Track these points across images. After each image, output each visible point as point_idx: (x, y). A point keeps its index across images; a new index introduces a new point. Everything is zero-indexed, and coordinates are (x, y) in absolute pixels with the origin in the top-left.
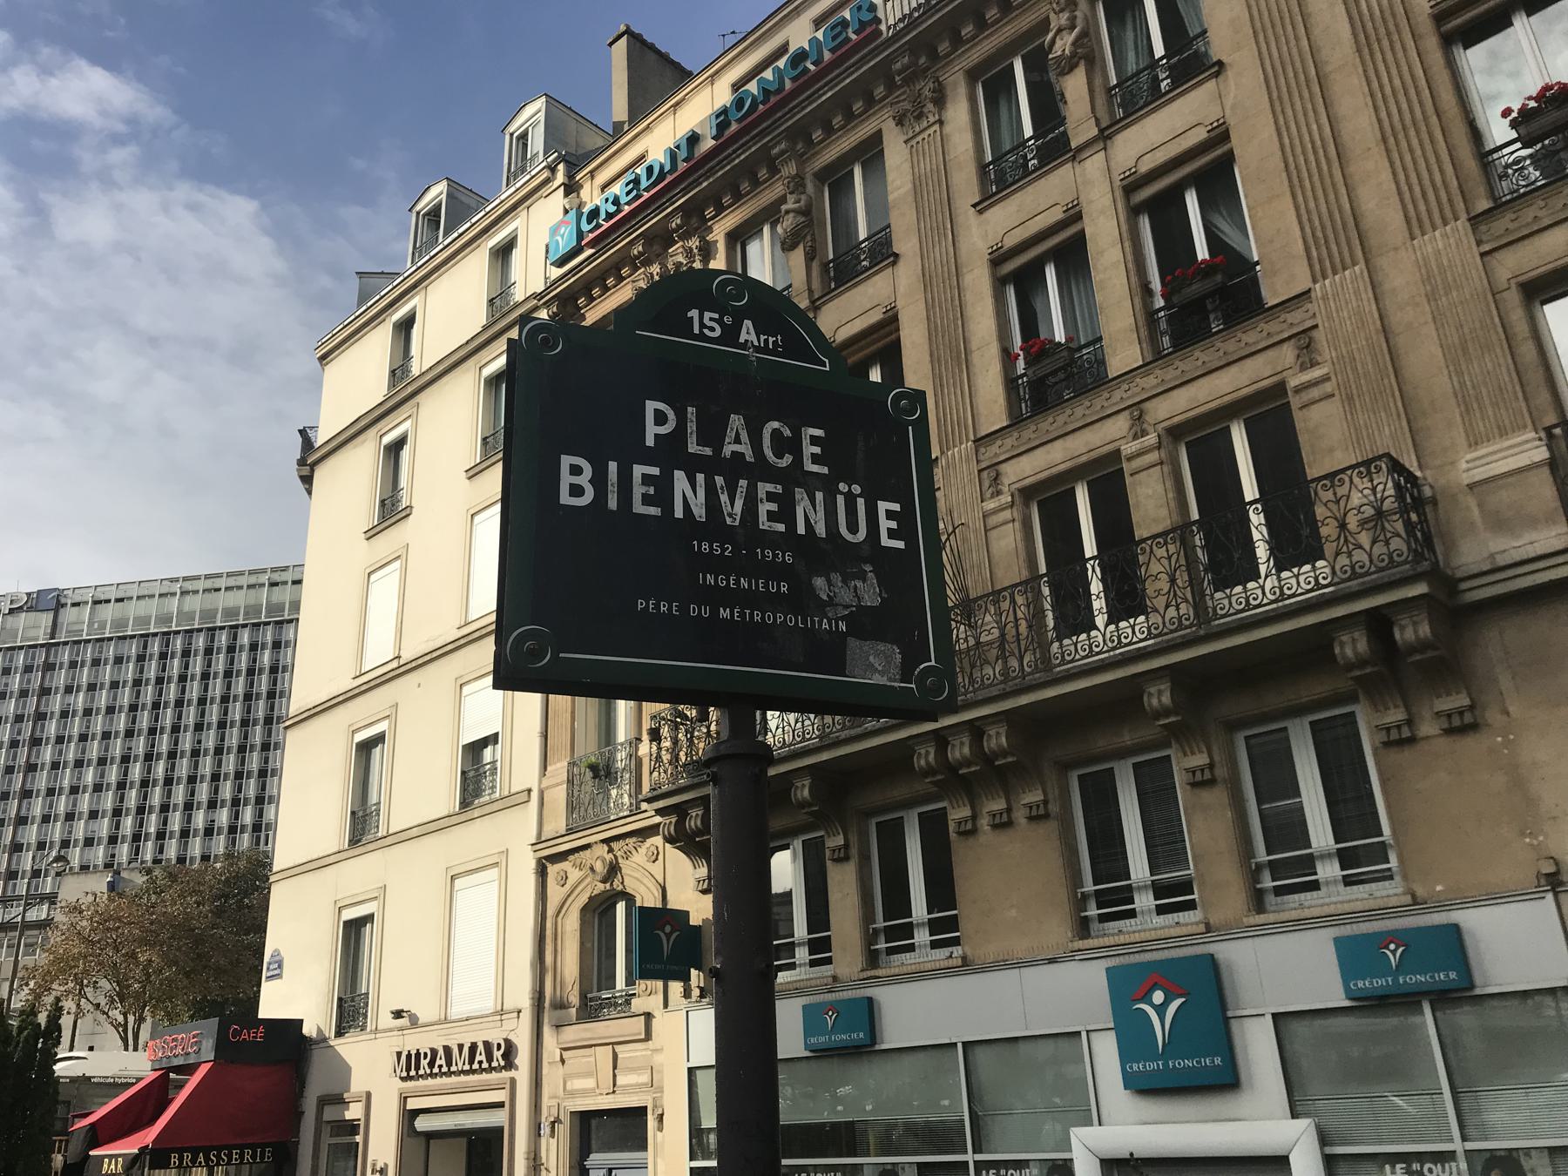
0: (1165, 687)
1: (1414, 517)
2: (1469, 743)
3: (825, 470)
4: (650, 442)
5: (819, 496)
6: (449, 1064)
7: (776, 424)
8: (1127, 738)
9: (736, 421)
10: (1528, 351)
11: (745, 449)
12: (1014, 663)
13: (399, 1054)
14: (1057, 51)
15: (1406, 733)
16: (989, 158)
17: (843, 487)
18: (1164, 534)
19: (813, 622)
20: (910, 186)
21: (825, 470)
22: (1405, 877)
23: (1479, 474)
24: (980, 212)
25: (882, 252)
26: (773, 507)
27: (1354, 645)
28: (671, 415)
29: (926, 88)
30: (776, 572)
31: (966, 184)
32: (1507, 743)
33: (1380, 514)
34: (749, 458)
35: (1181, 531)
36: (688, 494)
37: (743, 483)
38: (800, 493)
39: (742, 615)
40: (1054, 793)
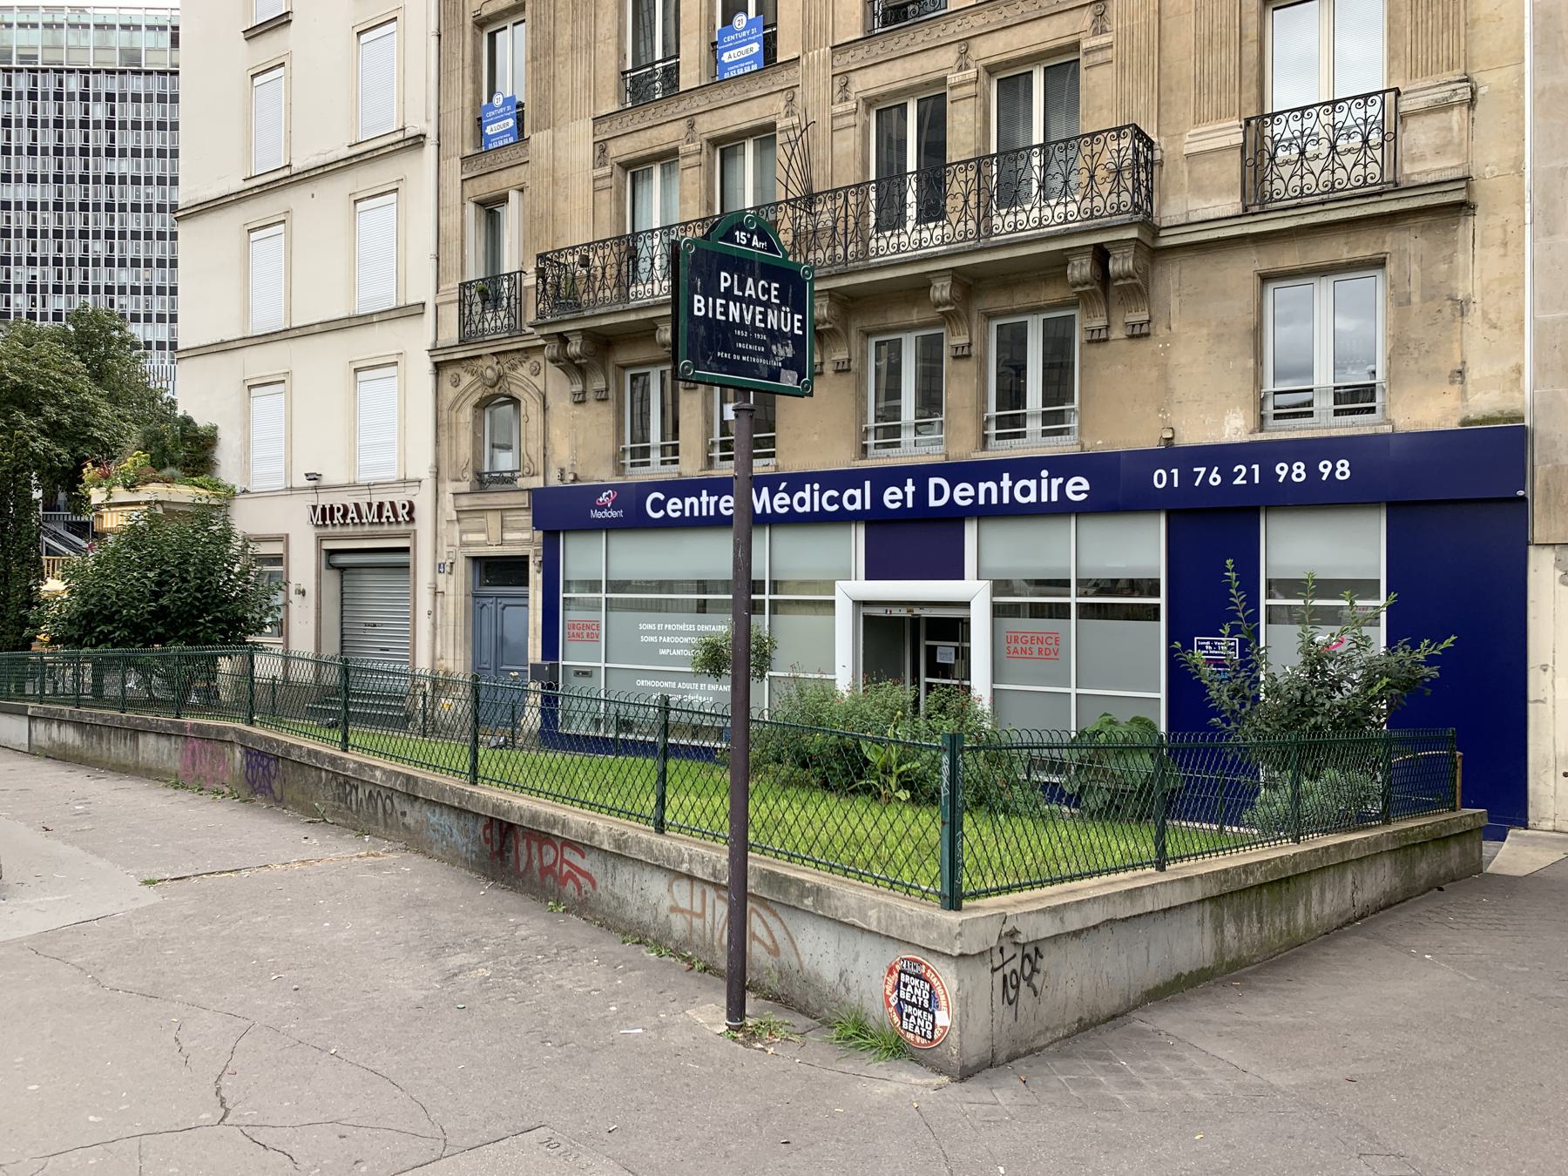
0: (947, 282)
1: (1143, 176)
2: (1141, 345)
6: (360, 517)
8: (915, 316)
9: (750, 280)
10: (1251, 50)
12: (840, 250)
13: (314, 508)
15: (1103, 336)
18: (967, 162)
22: (1080, 434)
23: (1194, 148)
27: (1081, 269)
30: (760, 343)
32: (1165, 349)
33: (1119, 172)
35: (981, 161)
36: (734, 311)
40: (856, 354)
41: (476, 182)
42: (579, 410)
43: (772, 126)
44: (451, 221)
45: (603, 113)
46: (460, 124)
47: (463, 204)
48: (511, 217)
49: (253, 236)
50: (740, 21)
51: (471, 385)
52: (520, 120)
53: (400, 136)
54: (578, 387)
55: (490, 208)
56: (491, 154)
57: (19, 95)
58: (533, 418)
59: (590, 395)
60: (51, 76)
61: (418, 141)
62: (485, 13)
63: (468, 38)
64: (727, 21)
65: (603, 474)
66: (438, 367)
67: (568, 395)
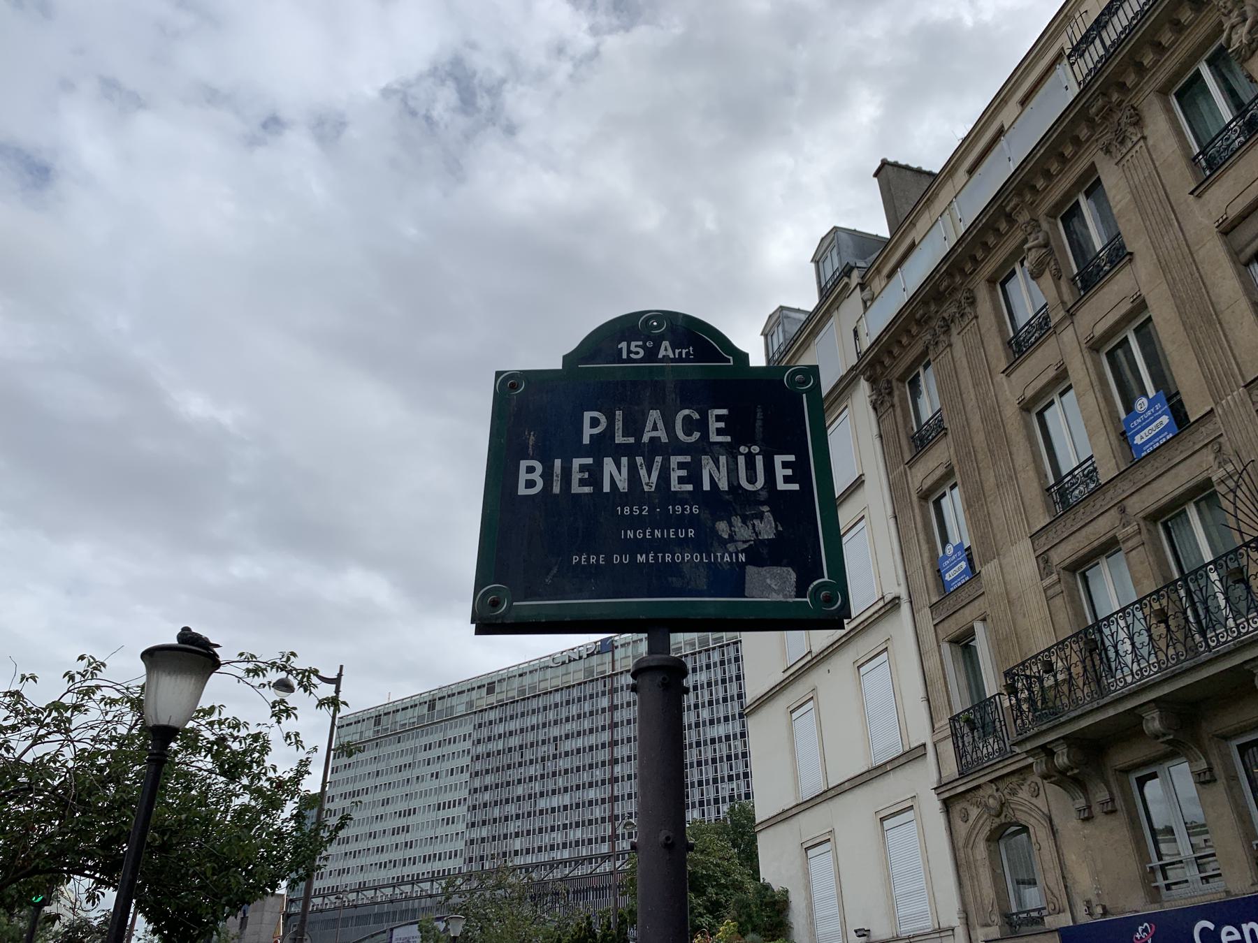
3: (728, 439)
4: (586, 440)
5: (723, 459)
7: (686, 412)
9: (654, 415)
11: (662, 434)
14: (1235, 44)
16: (1196, 150)
17: (743, 449)
19: (716, 557)
20: (1129, 196)
21: (728, 439)
24: (1199, 196)
25: (1119, 254)
26: (683, 473)
28: (603, 419)
29: (1123, 117)
30: (692, 521)
31: (1180, 178)
34: (665, 439)
36: (614, 473)
37: (659, 459)
38: (706, 461)
39: (656, 558)
41: (946, 624)
42: (1088, 829)
43: (1208, 483)
44: (932, 663)
45: (1039, 528)
46: (925, 578)
47: (939, 646)
48: (982, 644)
49: (795, 715)
50: (1141, 404)
51: (979, 817)
52: (970, 561)
53: (881, 604)
54: (1081, 803)
55: (964, 643)
56: (952, 596)
57: (715, 664)
58: (1044, 844)
59: (1096, 809)
60: (731, 648)
61: (895, 603)
62: (925, 487)
63: (917, 511)
64: (1129, 408)
65: (1134, 903)
66: (947, 804)
67: (1075, 814)
